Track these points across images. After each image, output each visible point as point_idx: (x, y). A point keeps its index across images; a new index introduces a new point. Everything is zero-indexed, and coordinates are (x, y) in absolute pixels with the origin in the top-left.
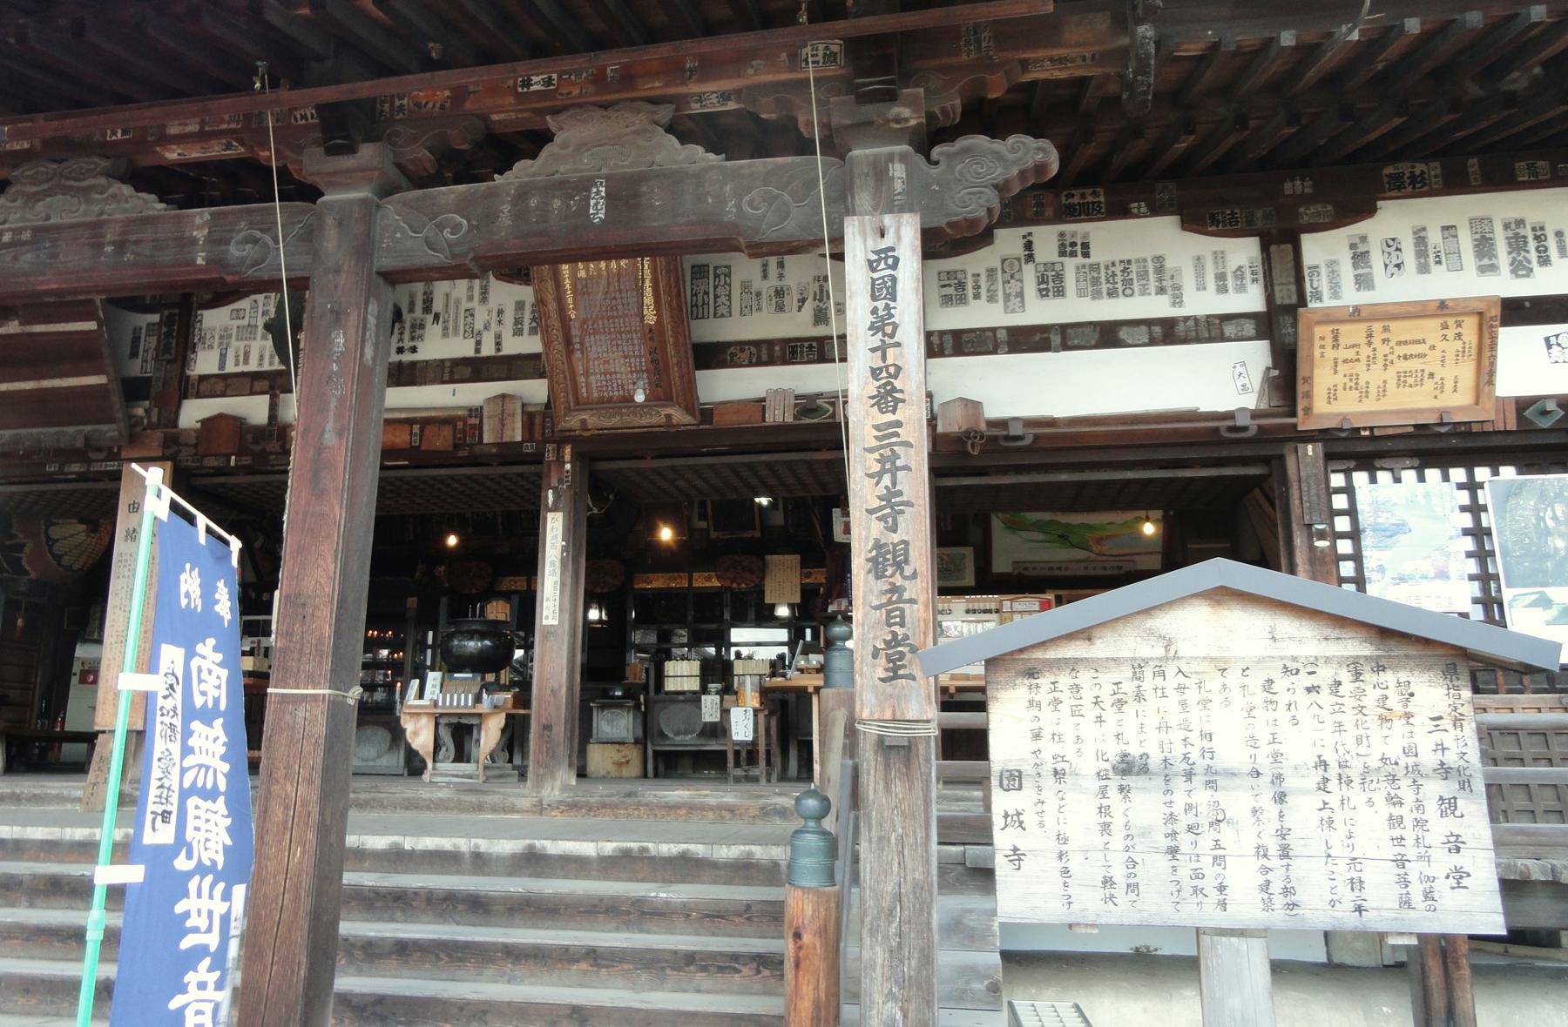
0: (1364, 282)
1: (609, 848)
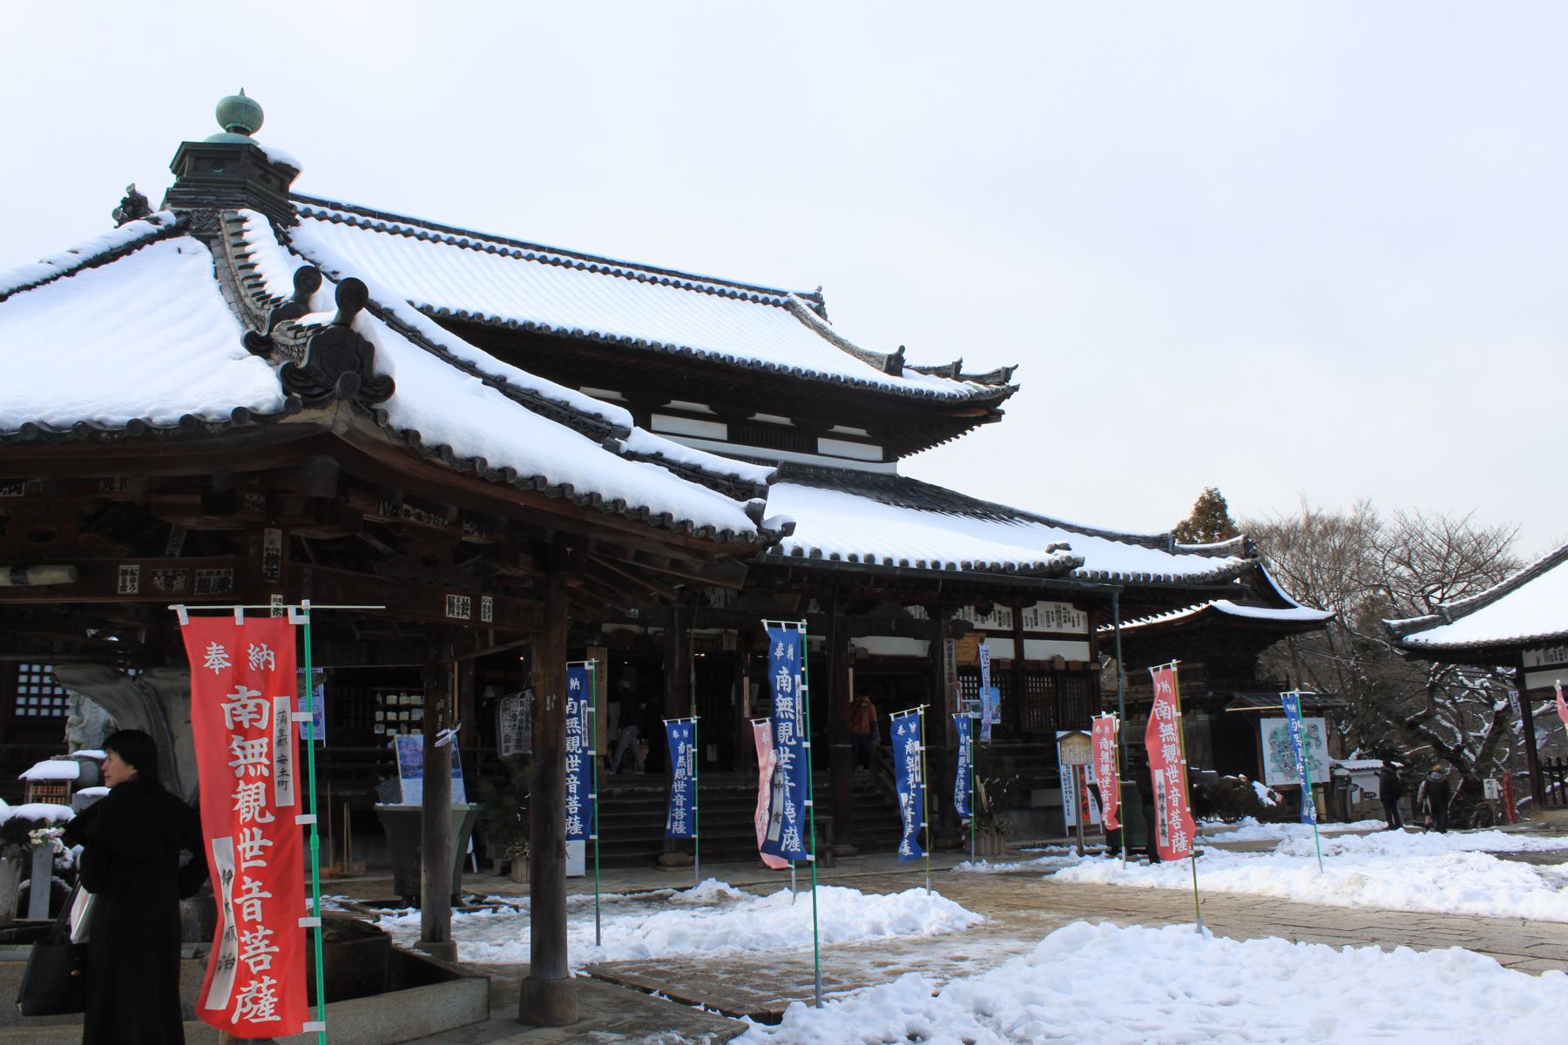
0: (1059, 625)
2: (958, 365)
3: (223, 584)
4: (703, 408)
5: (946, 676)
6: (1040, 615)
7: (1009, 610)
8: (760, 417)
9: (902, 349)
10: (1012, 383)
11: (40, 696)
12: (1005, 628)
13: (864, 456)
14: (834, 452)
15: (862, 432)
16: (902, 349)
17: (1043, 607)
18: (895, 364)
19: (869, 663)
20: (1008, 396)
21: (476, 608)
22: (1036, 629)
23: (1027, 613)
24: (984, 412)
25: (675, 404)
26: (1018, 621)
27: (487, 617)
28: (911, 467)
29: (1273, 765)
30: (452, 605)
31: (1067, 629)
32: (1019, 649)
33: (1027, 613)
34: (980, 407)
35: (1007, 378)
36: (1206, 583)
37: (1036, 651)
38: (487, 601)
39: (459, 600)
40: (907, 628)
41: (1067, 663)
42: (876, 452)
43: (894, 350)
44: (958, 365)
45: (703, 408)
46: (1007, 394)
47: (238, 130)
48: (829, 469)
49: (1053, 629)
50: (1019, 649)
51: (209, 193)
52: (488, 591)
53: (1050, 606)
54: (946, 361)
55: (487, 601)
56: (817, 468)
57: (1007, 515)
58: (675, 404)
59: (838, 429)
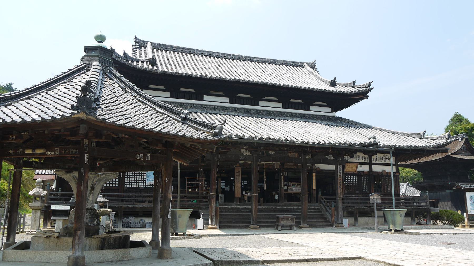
0: (385, 161)
1: (243, 207)
2: (354, 83)
3: (76, 152)
4: (275, 99)
5: (339, 176)
6: (378, 158)
7: (368, 156)
8: (292, 100)
9: (335, 78)
10: (371, 87)
11: (139, 178)
12: (366, 162)
13: (326, 111)
14: (315, 110)
15: (325, 104)
16: (335, 78)
17: (379, 155)
18: (333, 84)
19: (319, 172)
20: (370, 91)
21: (145, 156)
22: (377, 162)
23: (373, 157)
24: (362, 96)
25: (266, 98)
26: (370, 160)
27: (148, 159)
28: (340, 114)
29: (471, 207)
30: (137, 156)
31: (388, 162)
32: (371, 168)
33: (373, 157)
34: (362, 95)
35: (370, 85)
36: (433, 148)
37: (376, 169)
38: (148, 155)
39: (139, 155)
40: (330, 163)
41: (387, 173)
42: (329, 109)
43: (333, 79)
44: (354, 83)
45: (275, 99)
46: (370, 90)
47: (99, 42)
48: (313, 115)
49: (383, 162)
50: (371, 168)
51: (90, 58)
52: (148, 153)
53: (382, 155)
54: (351, 81)
55: (148, 155)
56: (310, 115)
57: (370, 127)
58: (266, 98)
59: (316, 103)
